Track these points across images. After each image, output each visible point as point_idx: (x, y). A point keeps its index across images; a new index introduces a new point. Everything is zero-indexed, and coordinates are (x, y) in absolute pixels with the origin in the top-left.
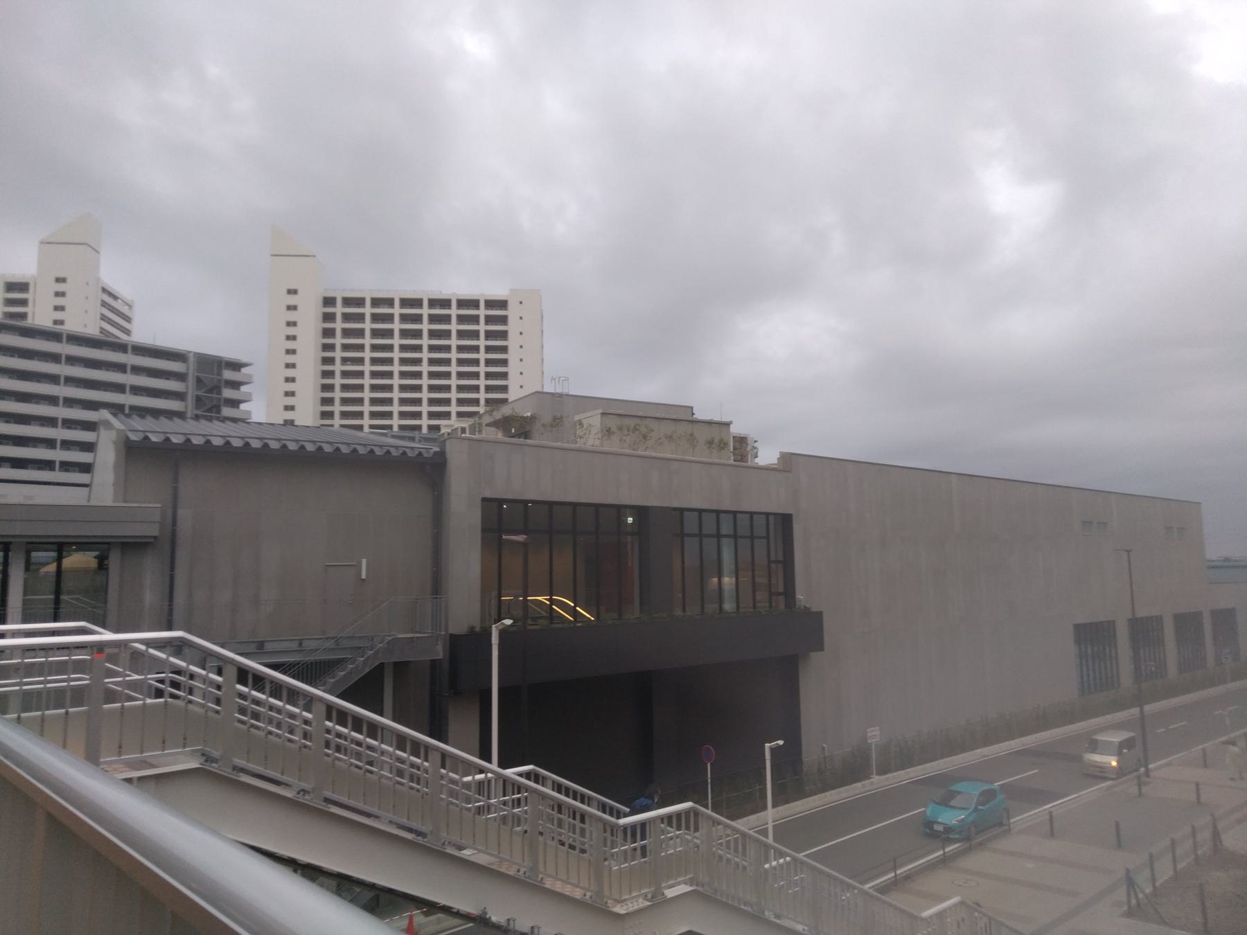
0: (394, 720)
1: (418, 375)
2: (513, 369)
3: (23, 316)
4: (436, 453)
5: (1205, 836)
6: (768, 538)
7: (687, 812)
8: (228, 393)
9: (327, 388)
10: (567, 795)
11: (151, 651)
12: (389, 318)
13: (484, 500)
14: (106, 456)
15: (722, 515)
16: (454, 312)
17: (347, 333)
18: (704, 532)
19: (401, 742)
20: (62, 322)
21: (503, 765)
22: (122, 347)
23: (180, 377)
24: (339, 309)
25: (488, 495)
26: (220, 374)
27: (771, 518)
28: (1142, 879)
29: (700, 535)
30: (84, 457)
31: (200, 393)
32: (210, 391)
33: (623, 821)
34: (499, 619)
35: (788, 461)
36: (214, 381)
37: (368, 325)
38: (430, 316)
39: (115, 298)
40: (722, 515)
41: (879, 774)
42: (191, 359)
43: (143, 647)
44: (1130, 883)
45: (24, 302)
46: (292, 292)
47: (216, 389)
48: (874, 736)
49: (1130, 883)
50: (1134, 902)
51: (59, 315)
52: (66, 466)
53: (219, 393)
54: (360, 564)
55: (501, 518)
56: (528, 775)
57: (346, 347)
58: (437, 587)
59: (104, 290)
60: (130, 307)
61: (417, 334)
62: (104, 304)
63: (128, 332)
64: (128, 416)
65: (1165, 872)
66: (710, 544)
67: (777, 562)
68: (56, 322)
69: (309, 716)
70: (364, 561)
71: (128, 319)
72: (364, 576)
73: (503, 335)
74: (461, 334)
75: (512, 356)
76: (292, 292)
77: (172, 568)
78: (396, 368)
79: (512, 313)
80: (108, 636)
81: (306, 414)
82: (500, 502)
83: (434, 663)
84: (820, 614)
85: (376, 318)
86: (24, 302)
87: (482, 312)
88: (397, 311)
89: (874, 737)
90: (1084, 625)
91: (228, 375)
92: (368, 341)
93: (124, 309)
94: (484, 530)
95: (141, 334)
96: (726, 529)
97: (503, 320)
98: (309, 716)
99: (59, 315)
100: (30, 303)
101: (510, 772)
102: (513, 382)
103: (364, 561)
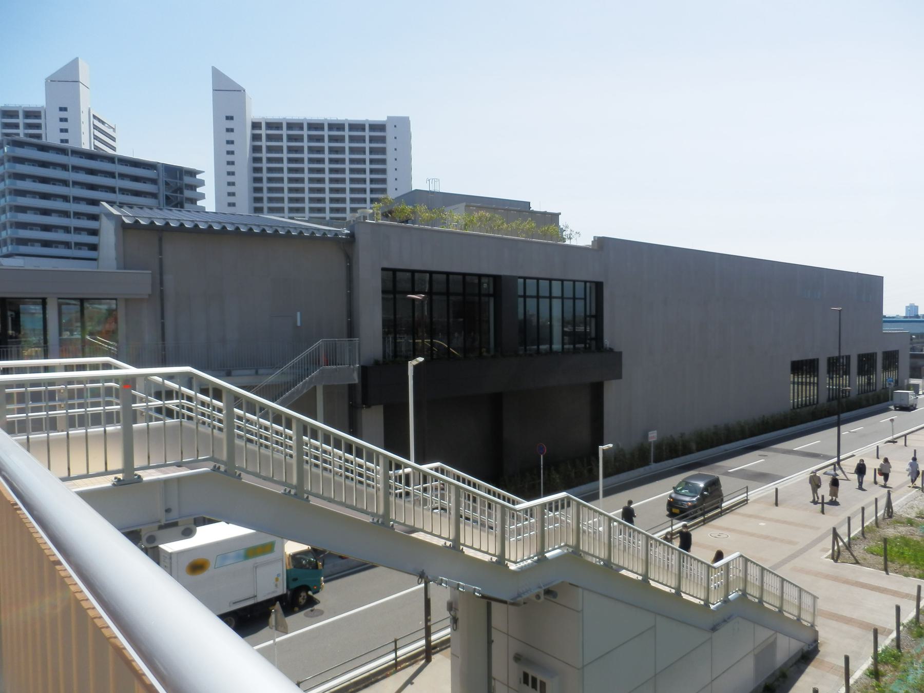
0: (386, 448)
1: (301, 180)
2: (390, 176)
3: (39, 137)
4: (347, 235)
5: (882, 503)
6: (585, 299)
7: (562, 499)
8: (187, 193)
9: (258, 190)
10: (499, 498)
11: (166, 382)
12: (299, 138)
13: (383, 269)
14: (108, 236)
15: (553, 282)
16: (347, 133)
17: (270, 149)
18: (528, 294)
19: (327, 438)
20: (66, 141)
21: (421, 460)
22: (111, 159)
23: (154, 181)
24: (263, 132)
25: (386, 265)
26: (181, 179)
27: (588, 284)
28: (843, 531)
29: (538, 297)
30: (91, 239)
31: (168, 194)
32: (175, 191)
33: (518, 507)
34: (414, 357)
35: (602, 243)
36: (176, 184)
37: (306, 144)
38: (350, 137)
39: (103, 123)
40: (553, 282)
41: (656, 461)
42: (161, 169)
43: (160, 379)
44: (836, 535)
45: (38, 126)
46: (229, 118)
47: (180, 190)
48: (653, 436)
49: (836, 535)
50: (836, 548)
51: (64, 136)
52: (79, 245)
53: (182, 193)
54: (296, 315)
55: (395, 283)
56: (436, 470)
57: (270, 160)
58: (351, 330)
59: (95, 117)
60: (114, 130)
61: (320, 150)
62: (96, 127)
63: (114, 149)
64: (121, 207)
65: (856, 530)
66: (544, 303)
67: (591, 316)
68: (62, 141)
69: (220, 404)
70: (299, 314)
71: (114, 139)
72: (299, 324)
73: (383, 151)
74: (352, 151)
75: (390, 166)
76: (229, 118)
77: (163, 317)
78: (306, 175)
79: (389, 134)
80: (131, 370)
81: (244, 206)
82: (394, 271)
83: (351, 387)
84: (620, 354)
85: (352, 139)
86: (38, 126)
87: (367, 134)
88: (305, 133)
89: (653, 437)
90: (798, 362)
91: (187, 180)
92: (306, 155)
93: (110, 131)
94: (384, 292)
95: (124, 149)
96: (556, 291)
97: (383, 140)
98: (220, 404)
99: (64, 136)
100: (43, 127)
101: (425, 467)
102: (390, 186)
103: (299, 314)
